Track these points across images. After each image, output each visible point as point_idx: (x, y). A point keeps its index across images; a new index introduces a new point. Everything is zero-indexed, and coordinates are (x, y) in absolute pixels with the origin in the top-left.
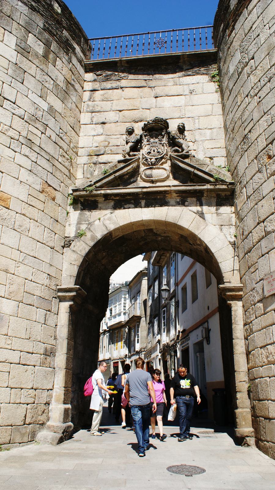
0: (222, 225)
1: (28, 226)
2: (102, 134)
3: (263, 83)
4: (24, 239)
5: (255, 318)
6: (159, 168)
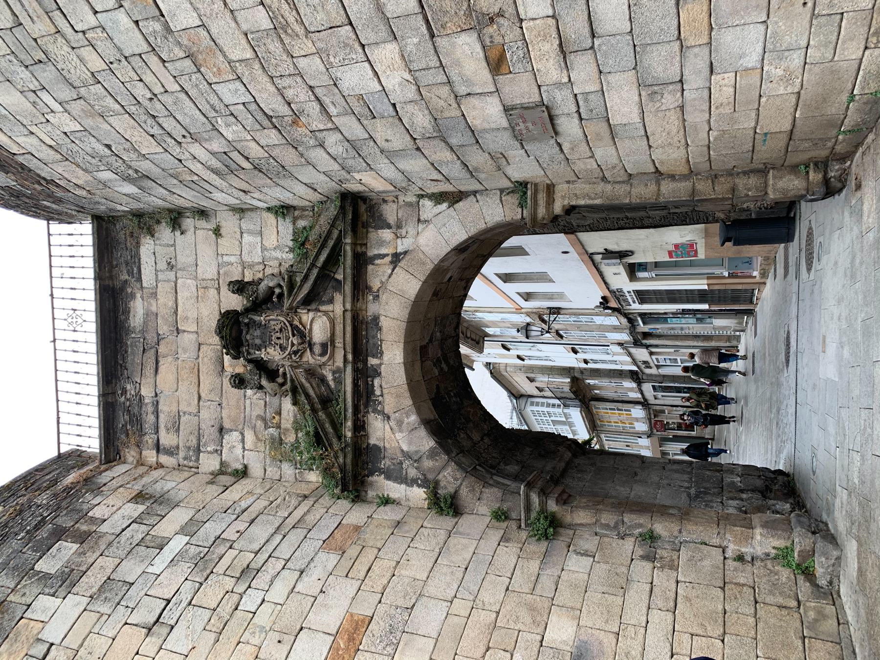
0: (419, 220)
1: (407, 580)
2: (242, 434)
3: (156, 131)
4: (431, 589)
5: (592, 160)
6: (311, 330)
